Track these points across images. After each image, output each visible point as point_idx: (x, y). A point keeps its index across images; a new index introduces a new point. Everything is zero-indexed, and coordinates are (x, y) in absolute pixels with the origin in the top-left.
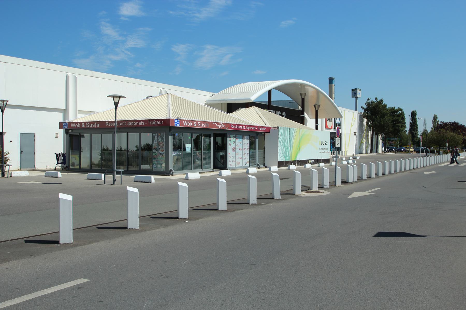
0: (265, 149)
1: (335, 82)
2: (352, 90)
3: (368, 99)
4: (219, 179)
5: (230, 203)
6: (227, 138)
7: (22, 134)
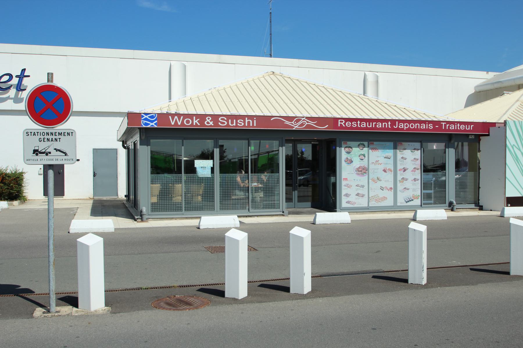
0: (480, 170)
4: (413, 225)
5: (500, 270)
6: (338, 148)
7: (95, 151)
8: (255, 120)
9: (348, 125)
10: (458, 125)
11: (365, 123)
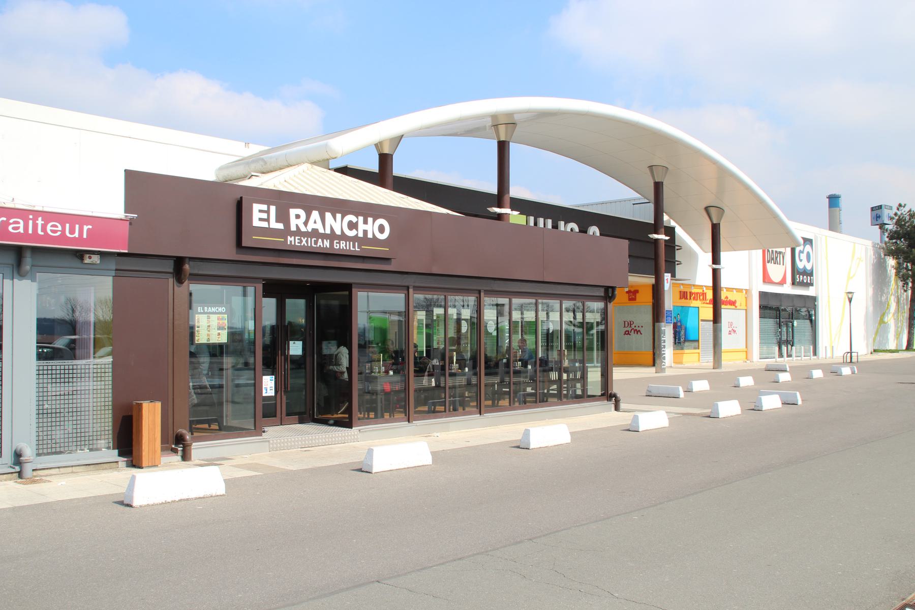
1: (843, 202)
2: (872, 209)
3: (900, 205)
8: (31, 219)
9: (52, 231)
10: (40, 222)
11: (22, 222)
